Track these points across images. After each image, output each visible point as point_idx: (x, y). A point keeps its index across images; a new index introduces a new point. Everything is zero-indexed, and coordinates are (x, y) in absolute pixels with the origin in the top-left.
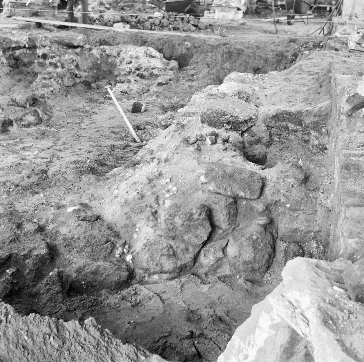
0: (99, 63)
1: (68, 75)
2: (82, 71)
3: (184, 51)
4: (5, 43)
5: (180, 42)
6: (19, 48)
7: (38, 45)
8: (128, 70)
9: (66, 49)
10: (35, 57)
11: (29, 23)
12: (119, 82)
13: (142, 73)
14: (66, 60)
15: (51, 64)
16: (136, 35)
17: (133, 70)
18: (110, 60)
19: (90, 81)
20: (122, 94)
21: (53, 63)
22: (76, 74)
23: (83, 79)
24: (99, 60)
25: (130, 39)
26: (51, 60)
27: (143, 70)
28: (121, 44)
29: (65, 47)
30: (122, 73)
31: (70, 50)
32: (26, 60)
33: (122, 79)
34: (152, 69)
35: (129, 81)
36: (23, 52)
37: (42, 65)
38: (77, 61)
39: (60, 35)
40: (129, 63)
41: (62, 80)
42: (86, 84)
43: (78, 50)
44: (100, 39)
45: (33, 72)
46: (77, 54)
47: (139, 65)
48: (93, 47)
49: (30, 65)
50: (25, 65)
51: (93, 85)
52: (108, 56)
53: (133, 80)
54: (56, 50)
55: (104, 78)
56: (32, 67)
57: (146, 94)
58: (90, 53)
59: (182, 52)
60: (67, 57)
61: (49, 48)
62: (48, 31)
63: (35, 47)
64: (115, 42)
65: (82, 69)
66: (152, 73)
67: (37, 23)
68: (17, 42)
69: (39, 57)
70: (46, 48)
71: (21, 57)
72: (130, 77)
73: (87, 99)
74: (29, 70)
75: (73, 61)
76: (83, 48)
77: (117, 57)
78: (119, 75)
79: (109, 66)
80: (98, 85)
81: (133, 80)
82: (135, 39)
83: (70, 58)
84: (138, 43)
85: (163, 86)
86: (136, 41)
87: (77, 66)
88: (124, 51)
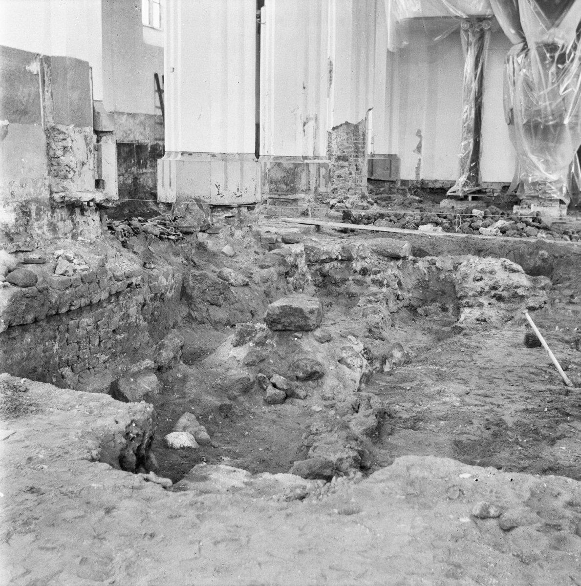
3: (539, 263)
4: (312, 254)
5: (531, 250)
6: (331, 260)
7: (355, 256)
8: (479, 290)
13: (499, 293)
16: (466, 241)
17: (487, 289)
18: (442, 276)
19: (416, 304)
21: (378, 280)
23: (406, 302)
27: (501, 289)
28: (445, 253)
29: (386, 259)
30: (470, 294)
31: (392, 263)
32: (338, 277)
33: (471, 301)
34: (516, 287)
35: (481, 305)
37: (358, 283)
43: (400, 262)
45: (348, 293)
47: (496, 282)
48: (418, 258)
50: (336, 283)
51: (420, 310)
52: (439, 270)
53: (486, 303)
55: (433, 301)
56: (346, 286)
57: (510, 322)
59: (535, 264)
63: (350, 259)
66: (516, 293)
68: (327, 253)
69: (355, 272)
71: (332, 273)
72: (481, 300)
74: (341, 289)
78: (466, 296)
79: (440, 284)
80: (426, 311)
81: (486, 303)
85: (536, 311)
86: (466, 249)
87: (399, 283)
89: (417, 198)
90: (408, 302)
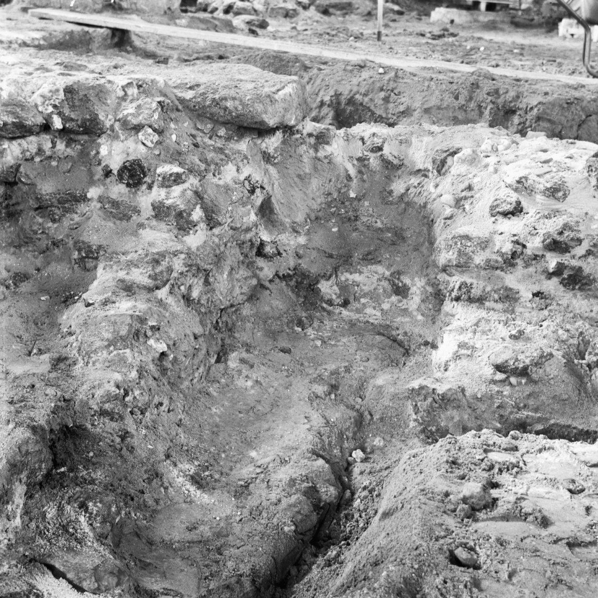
0: (352, 195)
1: (233, 255)
2: (284, 230)
7: (106, 119)
8: (508, 248)
9: (229, 139)
10: (91, 174)
11: (86, 29)
12: (458, 299)
13: (575, 263)
14: (227, 189)
15: (160, 211)
17: (535, 244)
18: (398, 187)
19: (314, 270)
20: (500, 376)
22: (262, 244)
23: (288, 263)
24: (354, 183)
25: (448, 100)
26: (163, 192)
27: (580, 251)
29: (222, 132)
30: (479, 259)
31: (243, 145)
32: (47, 188)
35: (509, 297)
36: (40, 151)
37: (119, 212)
38: (268, 188)
39: (203, 79)
40: (505, 214)
41: (207, 282)
42: (298, 285)
43: (272, 143)
44: (337, 95)
45: (79, 246)
46: (267, 158)
47: (566, 227)
49: (67, 211)
50: (42, 208)
51: (327, 288)
52: (392, 168)
54: (186, 143)
55: (370, 258)
56: (77, 218)
58: (321, 154)
60: (229, 174)
61: (156, 138)
62: (151, 61)
63: (91, 129)
64: (391, 105)
65: (287, 220)
67: (115, 31)
69: (108, 173)
70: (141, 135)
72: (511, 280)
73: (319, 379)
74: (57, 230)
75: (252, 191)
76: (293, 134)
77: (433, 174)
80: (344, 288)
82: (471, 99)
83: (242, 178)
84: (481, 114)
86: (472, 105)
87: (266, 210)
88: (466, 152)
89: (396, 8)
90: (292, 263)
